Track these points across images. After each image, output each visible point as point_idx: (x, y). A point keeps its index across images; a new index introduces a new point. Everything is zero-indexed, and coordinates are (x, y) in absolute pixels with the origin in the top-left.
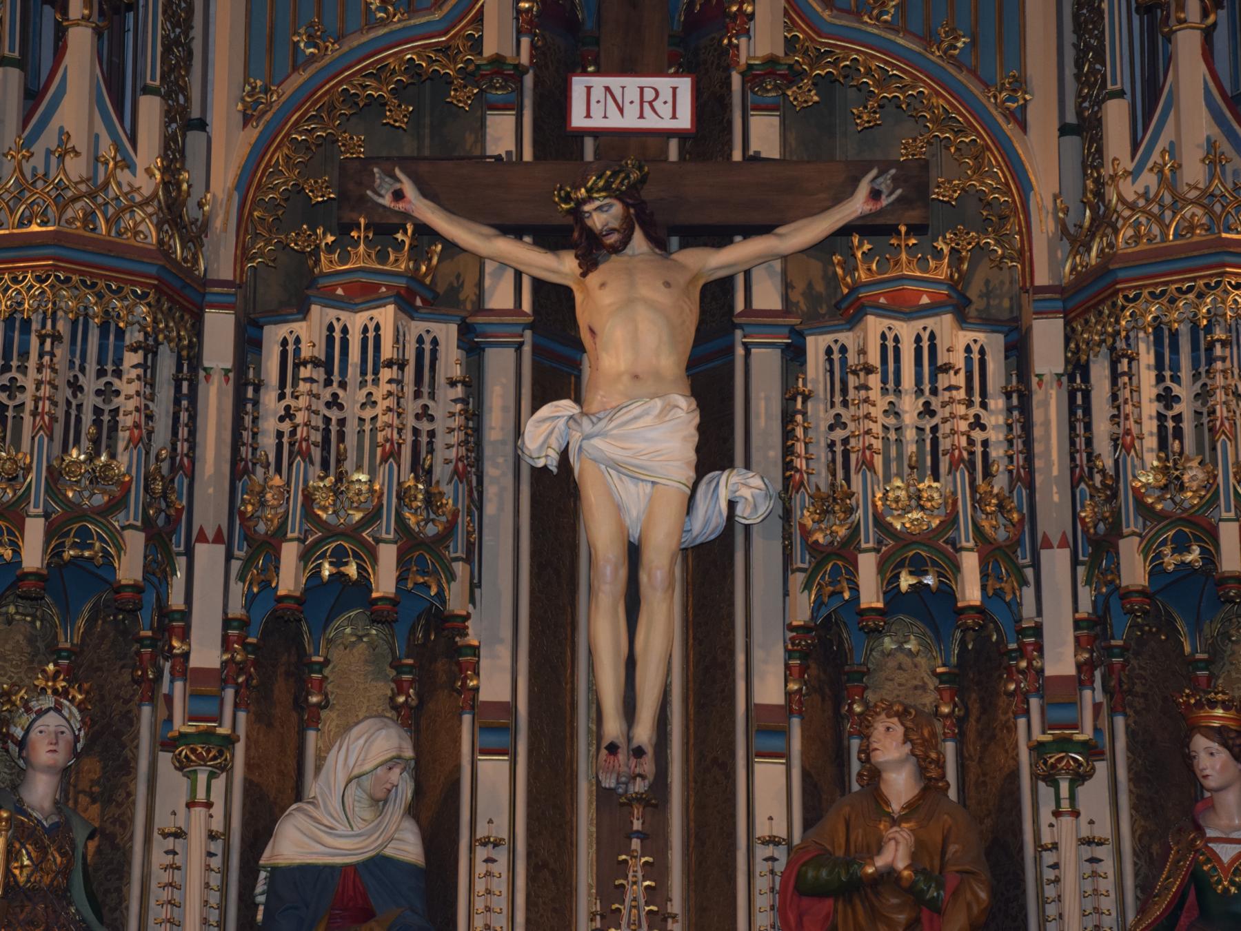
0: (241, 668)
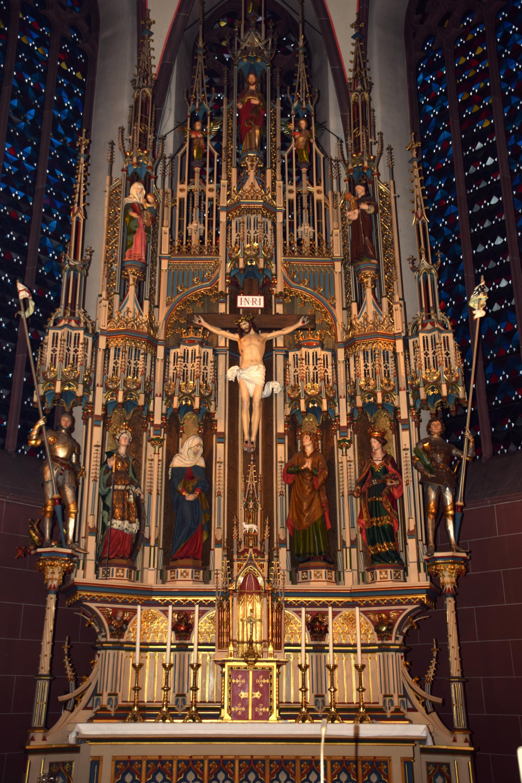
0: (165, 424)
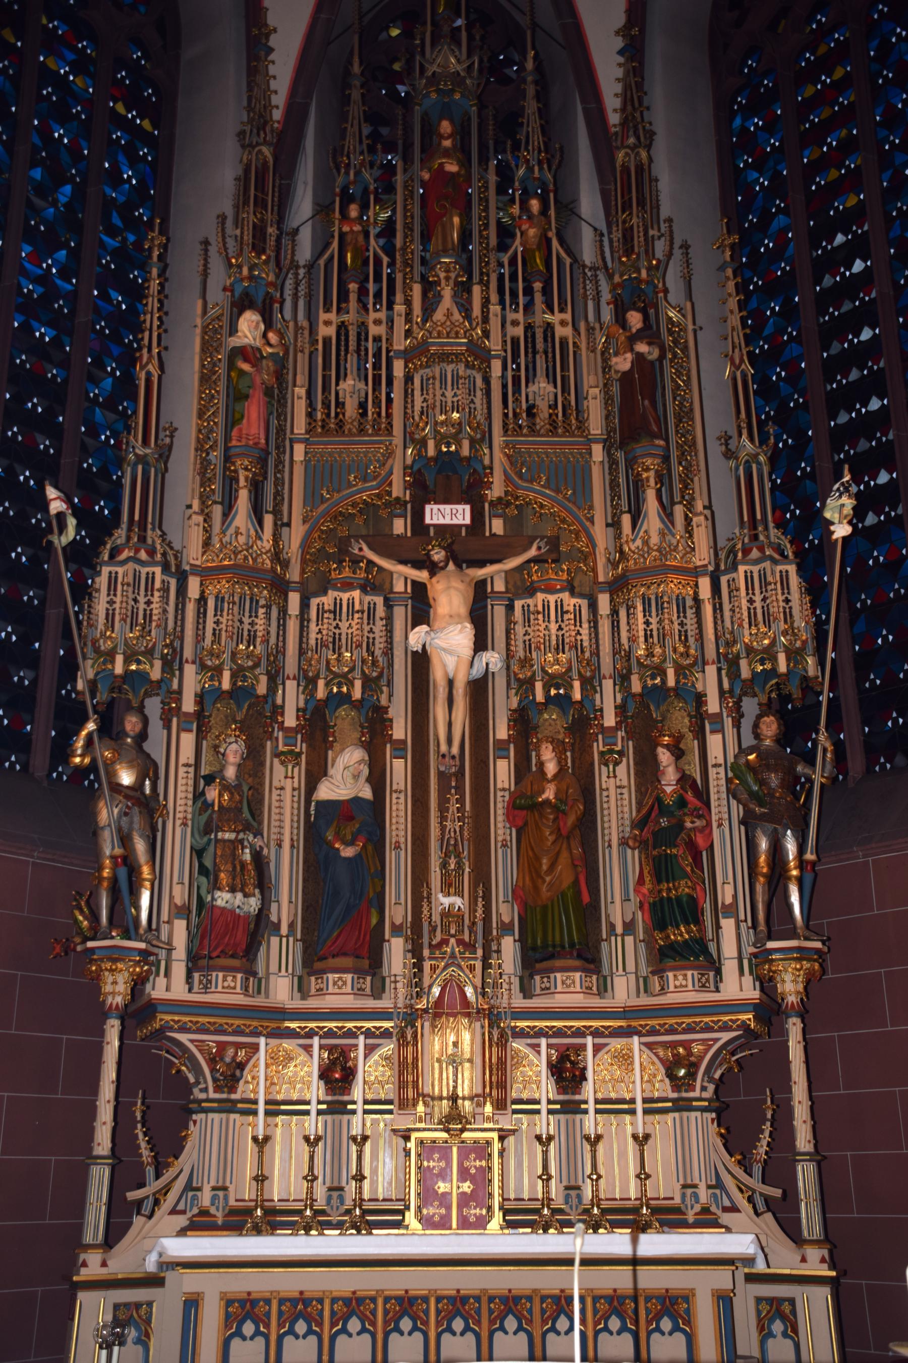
0: (303, 727)
